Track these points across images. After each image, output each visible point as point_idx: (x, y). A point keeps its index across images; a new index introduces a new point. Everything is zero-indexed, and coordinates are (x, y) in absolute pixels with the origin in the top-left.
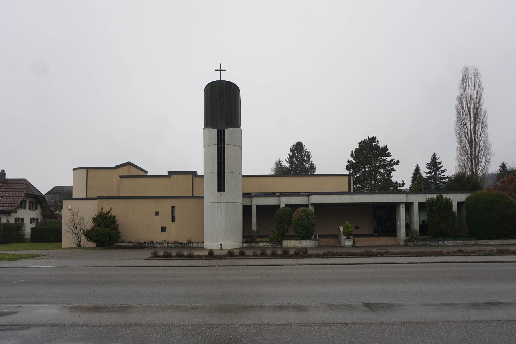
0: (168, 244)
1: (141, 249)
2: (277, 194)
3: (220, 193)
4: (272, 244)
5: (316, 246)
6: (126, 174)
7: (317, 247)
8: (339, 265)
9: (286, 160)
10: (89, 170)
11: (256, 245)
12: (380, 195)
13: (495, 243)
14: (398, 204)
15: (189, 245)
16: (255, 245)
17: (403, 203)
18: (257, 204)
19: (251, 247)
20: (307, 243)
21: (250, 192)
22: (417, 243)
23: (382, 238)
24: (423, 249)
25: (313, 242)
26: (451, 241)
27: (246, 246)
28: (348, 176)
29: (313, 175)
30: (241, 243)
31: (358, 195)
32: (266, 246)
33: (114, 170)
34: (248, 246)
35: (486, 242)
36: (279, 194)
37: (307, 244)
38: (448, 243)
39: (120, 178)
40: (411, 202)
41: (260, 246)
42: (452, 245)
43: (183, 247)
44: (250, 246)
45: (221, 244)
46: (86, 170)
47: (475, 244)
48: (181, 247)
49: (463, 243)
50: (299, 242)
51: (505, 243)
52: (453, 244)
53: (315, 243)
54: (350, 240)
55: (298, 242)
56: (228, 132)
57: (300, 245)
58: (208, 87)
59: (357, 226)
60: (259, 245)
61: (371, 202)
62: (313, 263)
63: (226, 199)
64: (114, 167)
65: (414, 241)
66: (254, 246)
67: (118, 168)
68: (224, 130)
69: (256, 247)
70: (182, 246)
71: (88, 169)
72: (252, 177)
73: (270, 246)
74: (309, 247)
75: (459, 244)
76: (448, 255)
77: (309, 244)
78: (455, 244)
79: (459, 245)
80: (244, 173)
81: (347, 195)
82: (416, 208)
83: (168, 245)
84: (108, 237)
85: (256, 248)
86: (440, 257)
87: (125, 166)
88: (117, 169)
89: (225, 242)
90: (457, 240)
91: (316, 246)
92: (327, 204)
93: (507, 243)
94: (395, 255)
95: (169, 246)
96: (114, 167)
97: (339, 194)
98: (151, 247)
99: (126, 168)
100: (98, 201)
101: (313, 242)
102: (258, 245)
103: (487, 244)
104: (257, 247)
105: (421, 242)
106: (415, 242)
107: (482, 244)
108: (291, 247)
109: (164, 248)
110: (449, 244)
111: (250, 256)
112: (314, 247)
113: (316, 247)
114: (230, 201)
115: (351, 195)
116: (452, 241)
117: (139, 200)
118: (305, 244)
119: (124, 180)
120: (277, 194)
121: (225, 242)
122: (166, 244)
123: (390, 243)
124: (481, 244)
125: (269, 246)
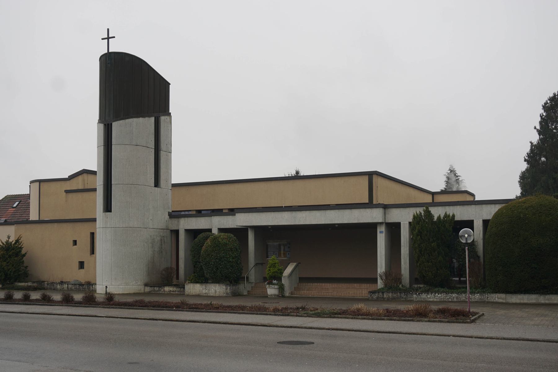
0: (68, 284)
1: (32, 291)
2: (224, 211)
3: (105, 214)
4: (179, 289)
5: (227, 294)
6: (81, 187)
7: (229, 295)
8: (88, 318)
9: (535, 128)
10: (42, 184)
11: (161, 290)
12: (337, 211)
13: (522, 301)
14: (372, 227)
15: (90, 288)
16: (159, 290)
17: (381, 223)
18: (484, 219)
19: (154, 292)
20: (216, 289)
21: (220, 208)
22: (383, 295)
23: (358, 285)
24: (392, 306)
25: (223, 288)
26: (435, 294)
27: (149, 290)
28: (369, 175)
29: (30, 194)
30: (143, 286)
31: (302, 212)
32: (173, 291)
33: (68, 182)
34: (151, 291)
35: (503, 299)
36: (194, 213)
37: (216, 291)
38: (430, 298)
39: (66, 193)
40: (397, 221)
41: (165, 292)
42: (436, 302)
43: (83, 290)
44: (154, 291)
45: (106, 287)
46: (38, 183)
47: (480, 300)
48: (81, 290)
49: (457, 298)
50: (205, 288)
51: (543, 302)
52: (438, 300)
53: (227, 289)
54: (271, 286)
55: (204, 287)
56: (163, 118)
57: (207, 291)
58: (102, 59)
59: (77, 265)
60: (164, 290)
61: (338, 222)
62: (355, 327)
63: (113, 223)
64: (68, 177)
65: (378, 292)
66: (158, 291)
67: (76, 177)
68: (111, 124)
69: (161, 292)
70: (83, 288)
71: (40, 181)
72: (337, 176)
73: (178, 291)
74: (218, 295)
75: (450, 300)
76: (259, 313)
77: (218, 291)
78: (442, 300)
79: (449, 301)
80: (173, 182)
81: (286, 212)
82: (182, 236)
83: (68, 286)
84: (3, 274)
85: (160, 293)
86: (19, 306)
87: (79, 175)
88: (72, 180)
89: (111, 284)
90: (447, 293)
91: (227, 294)
92: (337, 226)
93: (547, 302)
94: (367, 315)
95: (69, 288)
96: (68, 177)
97: (274, 212)
98: (40, 289)
99: (80, 178)
100: (15, 227)
101: (223, 288)
102: (162, 290)
103: (504, 301)
104: (162, 293)
105: (390, 295)
106: (381, 294)
107: (495, 301)
108: (195, 294)
109: (64, 290)
110: (432, 300)
111: (37, 300)
112: (225, 295)
113: (227, 295)
114: (118, 226)
115: (291, 212)
116: (437, 294)
117: (56, 224)
118: (212, 290)
119: (70, 195)
120: (224, 211)
121: (111, 284)
122: (66, 285)
123: (362, 293)
124: (493, 301)
125: (176, 291)
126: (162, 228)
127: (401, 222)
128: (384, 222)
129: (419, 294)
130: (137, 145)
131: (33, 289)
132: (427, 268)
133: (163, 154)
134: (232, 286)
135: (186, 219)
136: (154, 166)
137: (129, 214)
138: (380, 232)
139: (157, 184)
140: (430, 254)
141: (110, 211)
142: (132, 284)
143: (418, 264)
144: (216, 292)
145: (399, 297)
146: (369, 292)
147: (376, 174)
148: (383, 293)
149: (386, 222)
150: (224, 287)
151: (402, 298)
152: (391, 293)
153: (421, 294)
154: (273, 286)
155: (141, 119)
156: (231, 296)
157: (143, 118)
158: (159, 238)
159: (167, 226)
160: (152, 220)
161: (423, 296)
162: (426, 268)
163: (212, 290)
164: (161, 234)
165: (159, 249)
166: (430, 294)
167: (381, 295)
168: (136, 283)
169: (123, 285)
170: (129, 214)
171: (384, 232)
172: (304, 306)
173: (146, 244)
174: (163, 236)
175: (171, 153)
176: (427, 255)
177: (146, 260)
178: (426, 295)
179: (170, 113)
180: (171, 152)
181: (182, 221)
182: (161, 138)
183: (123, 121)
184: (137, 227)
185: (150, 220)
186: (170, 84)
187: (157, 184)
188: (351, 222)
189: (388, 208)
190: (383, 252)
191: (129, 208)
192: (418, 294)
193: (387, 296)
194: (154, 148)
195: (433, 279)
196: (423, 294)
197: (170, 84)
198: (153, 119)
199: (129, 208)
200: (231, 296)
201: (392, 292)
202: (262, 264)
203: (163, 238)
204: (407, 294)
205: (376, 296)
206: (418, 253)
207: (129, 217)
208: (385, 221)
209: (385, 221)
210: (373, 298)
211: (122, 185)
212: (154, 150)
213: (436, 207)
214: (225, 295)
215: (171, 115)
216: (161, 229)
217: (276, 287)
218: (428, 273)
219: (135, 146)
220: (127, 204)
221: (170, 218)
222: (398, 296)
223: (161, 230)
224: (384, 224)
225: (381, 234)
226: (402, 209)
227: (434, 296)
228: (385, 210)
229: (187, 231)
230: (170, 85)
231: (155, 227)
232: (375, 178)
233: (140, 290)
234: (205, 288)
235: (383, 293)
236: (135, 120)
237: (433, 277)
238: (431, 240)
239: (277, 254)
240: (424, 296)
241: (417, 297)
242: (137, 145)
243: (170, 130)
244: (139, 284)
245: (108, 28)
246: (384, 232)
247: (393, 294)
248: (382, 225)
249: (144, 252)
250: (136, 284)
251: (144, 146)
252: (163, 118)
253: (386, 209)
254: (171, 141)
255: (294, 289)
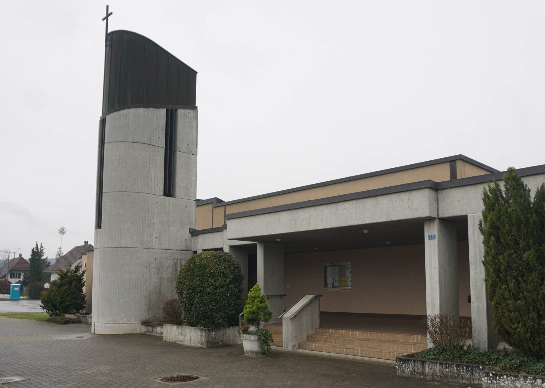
17: (430, 219)
22: (423, 367)
26: (535, 379)
40: (459, 214)
41: (157, 333)
44: (148, 332)
50: (181, 332)
56: (181, 112)
65: (414, 361)
105: (438, 368)
106: (418, 365)
114: (106, 246)
121: (98, 321)
126: (177, 249)
129: (495, 375)
130: (134, 142)
131: (64, 322)
132: (515, 312)
134: (207, 331)
135: (204, 235)
138: (429, 236)
140: (520, 279)
141: (100, 228)
142: (121, 322)
143: (493, 303)
144: (191, 340)
145: (455, 375)
146: (396, 358)
147: (461, 159)
148: (423, 363)
149: (440, 217)
150: (199, 333)
151: (463, 378)
152: (438, 365)
153: (500, 378)
154: (248, 336)
155: (141, 110)
156: (206, 347)
157: (145, 109)
158: (171, 262)
159: (187, 246)
160: (158, 238)
161: (504, 382)
162: (510, 312)
163: (188, 336)
164: (176, 256)
165: (172, 276)
166: (522, 379)
167: (419, 367)
168: (128, 321)
169: (110, 323)
173: (145, 269)
174: (179, 258)
176: (513, 280)
177: (145, 291)
178: (513, 382)
180: (195, 153)
181: (200, 239)
182: (178, 136)
183: (117, 112)
185: (154, 237)
188: (375, 221)
189: (444, 189)
191: (121, 222)
192: (491, 375)
193: (432, 371)
194: (164, 147)
195: (530, 340)
196: (505, 376)
198: (162, 112)
199: (121, 222)
200: (206, 347)
201: (441, 364)
202: (281, 296)
203: (179, 262)
204: (472, 369)
205: (409, 367)
206: (493, 277)
207: (121, 233)
208: (438, 215)
209: (438, 215)
210: (404, 373)
211: (113, 193)
212: (164, 149)
213: (539, 176)
214: (199, 345)
215: (197, 109)
217: (253, 337)
218: (516, 325)
220: (118, 217)
221: (192, 236)
222: (452, 371)
223: (175, 251)
224: (437, 222)
225: (432, 240)
226: (468, 188)
227: (532, 384)
228: (437, 194)
230: (197, 74)
231: (164, 247)
232: (459, 165)
233: (134, 330)
234: (181, 333)
235: (423, 363)
236: (132, 110)
237: (528, 335)
238: (522, 244)
239: (338, 281)
240: (506, 383)
241: (489, 382)
242: (134, 142)
243: (194, 127)
244: (132, 321)
245: (108, 5)
247: (444, 367)
248: (433, 222)
249: (142, 279)
250: (128, 322)
252: (181, 112)
253: (440, 192)
254: (197, 141)
255: (306, 338)
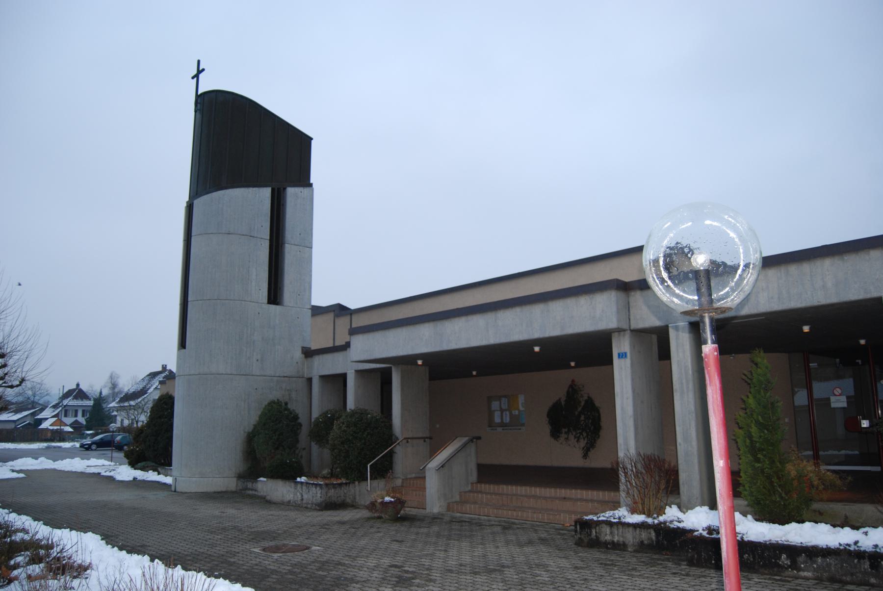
17: (620, 331)
56: (291, 191)
126: (285, 375)
127: (670, 325)
128: (625, 326)
133: (290, 253)
136: (267, 268)
137: (211, 351)
138: (619, 355)
139: (275, 296)
146: (576, 522)
149: (632, 328)
170: (211, 351)
171: (628, 355)
172: (748, 479)
174: (288, 388)
175: (312, 248)
179: (312, 184)
184: (224, 373)
186: (312, 139)
187: (275, 296)
190: (630, 410)
197: (312, 139)
198: (266, 192)
211: (201, 302)
216: (284, 377)
219: (226, 235)
223: (282, 378)
224: (628, 333)
225: (622, 360)
229: (324, 378)
230: (312, 141)
246: (628, 355)
251: (244, 234)
252: (291, 191)
